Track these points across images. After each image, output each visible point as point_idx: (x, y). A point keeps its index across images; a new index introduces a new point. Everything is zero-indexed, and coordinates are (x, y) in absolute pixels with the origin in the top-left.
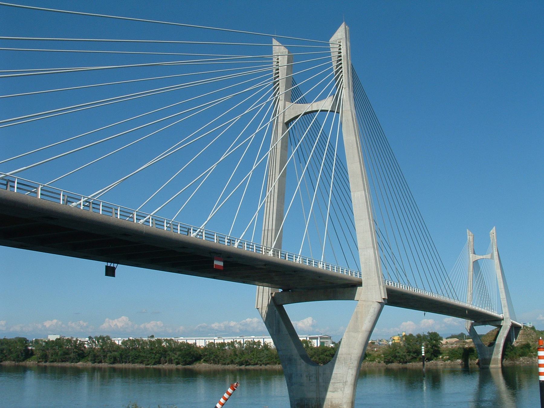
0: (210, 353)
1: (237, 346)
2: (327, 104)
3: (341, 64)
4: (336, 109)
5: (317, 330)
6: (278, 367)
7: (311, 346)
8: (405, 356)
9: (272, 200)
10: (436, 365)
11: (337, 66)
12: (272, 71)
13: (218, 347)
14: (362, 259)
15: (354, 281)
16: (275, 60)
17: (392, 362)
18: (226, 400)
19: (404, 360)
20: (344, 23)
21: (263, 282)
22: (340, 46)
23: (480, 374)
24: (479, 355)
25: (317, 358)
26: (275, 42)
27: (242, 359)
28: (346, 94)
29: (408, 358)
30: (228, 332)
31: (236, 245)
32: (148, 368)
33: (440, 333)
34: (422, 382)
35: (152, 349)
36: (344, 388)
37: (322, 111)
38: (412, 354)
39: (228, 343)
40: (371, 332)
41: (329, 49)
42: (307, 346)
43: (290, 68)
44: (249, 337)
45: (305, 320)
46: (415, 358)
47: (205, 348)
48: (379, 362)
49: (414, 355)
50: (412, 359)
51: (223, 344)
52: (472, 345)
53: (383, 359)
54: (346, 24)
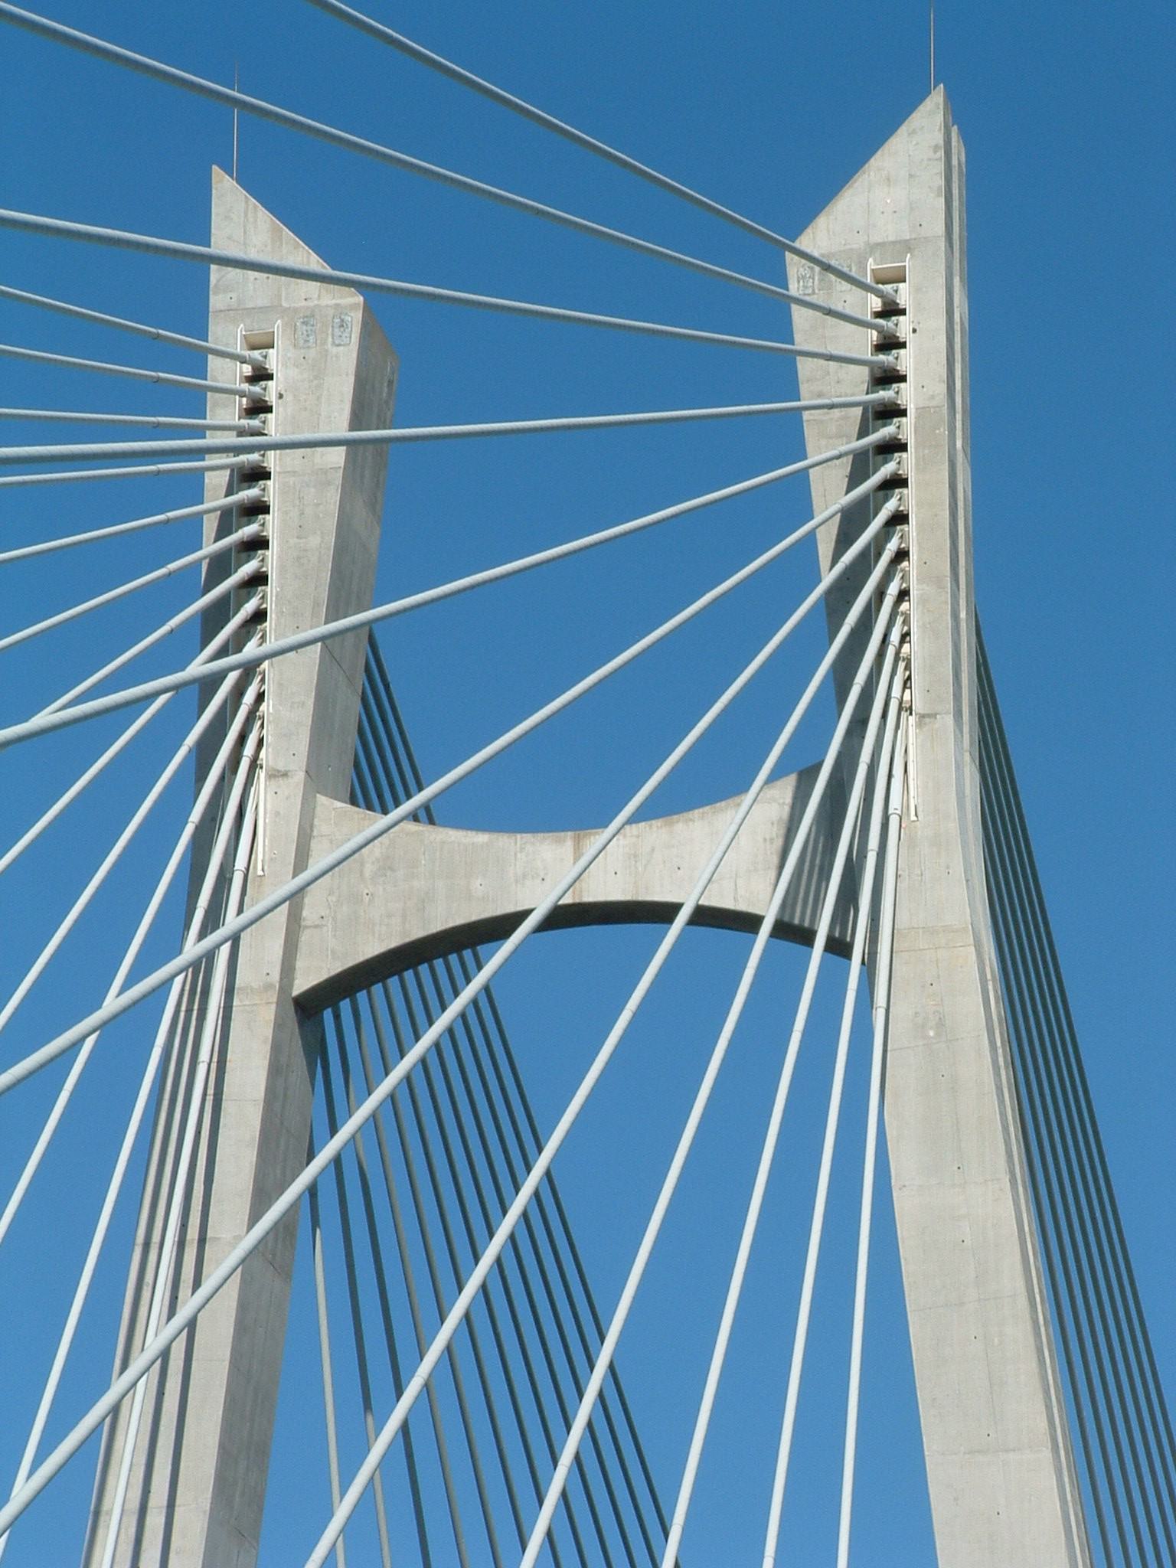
2: (726, 853)
3: (897, 482)
4: (823, 919)
12: (192, 487)
16: (226, 373)
26: (239, 220)
28: (924, 779)
37: (705, 916)
54: (957, 113)
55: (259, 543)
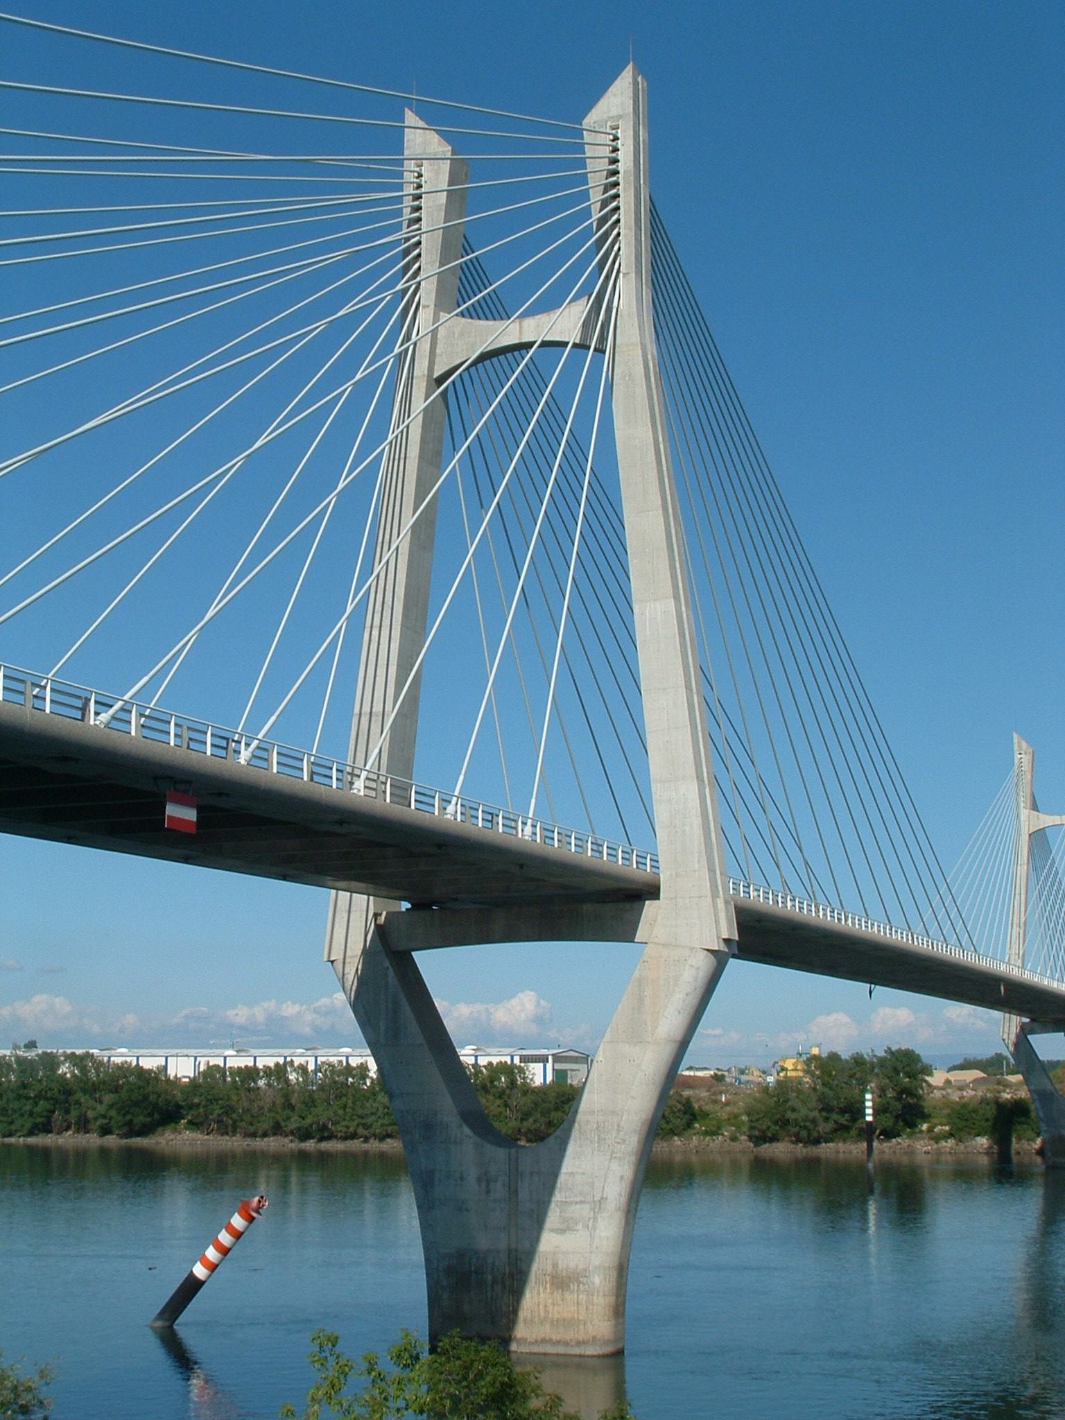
0: (210, 1101)
1: (292, 1077)
2: (565, 323)
4: (595, 340)
5: (552, 1034)
6: (392, 1146)
7: (525, 1084)
8: (814, 1121)
9: (386, 622)
10: (911, 1152)
11: (604, 204)
12: (399, 213)
13: (234, 1082)
14: (661, 814)
15: (632, 881)
17: (774, 1139)
18: (225, 1251)
19: (809, 1135)
20: (630, 67)
21: (357, 878)
22: (616, 139)
23: (1047, 1185)
24: (1043, 1126)
25: (542, 1120)
26: (411, 118)
27: (309, 1121)
28: (629, 296)
29: (824, 1127)
30: (276, 1033)
31: (244, 756)
32: (10, 1145)
33: (925, 1054)
34: (864, 1202)
35: (24, 1086)
36: (595, 1219)
37: (545, 344)
38: (835, 1116)
39: (267, 1068)
40: (684, 1044)
41: (580, 148)
42: (512, 1083)
43: (457, 201)
44: (333, 1051)
45: (514, 1002)
46: (846, 1128)
47: (193, 1081)
48: (734, 1139)
49: (843, 1120)
50: (836, 1130)
51: (250, 1074)
52: (1023, 1094)
53: (745, 1129)
54: (638, 70)
55: (617, 196)
